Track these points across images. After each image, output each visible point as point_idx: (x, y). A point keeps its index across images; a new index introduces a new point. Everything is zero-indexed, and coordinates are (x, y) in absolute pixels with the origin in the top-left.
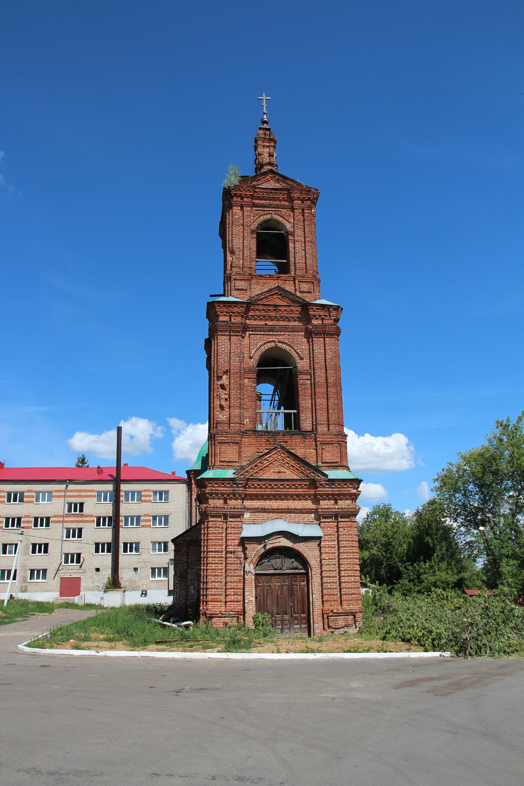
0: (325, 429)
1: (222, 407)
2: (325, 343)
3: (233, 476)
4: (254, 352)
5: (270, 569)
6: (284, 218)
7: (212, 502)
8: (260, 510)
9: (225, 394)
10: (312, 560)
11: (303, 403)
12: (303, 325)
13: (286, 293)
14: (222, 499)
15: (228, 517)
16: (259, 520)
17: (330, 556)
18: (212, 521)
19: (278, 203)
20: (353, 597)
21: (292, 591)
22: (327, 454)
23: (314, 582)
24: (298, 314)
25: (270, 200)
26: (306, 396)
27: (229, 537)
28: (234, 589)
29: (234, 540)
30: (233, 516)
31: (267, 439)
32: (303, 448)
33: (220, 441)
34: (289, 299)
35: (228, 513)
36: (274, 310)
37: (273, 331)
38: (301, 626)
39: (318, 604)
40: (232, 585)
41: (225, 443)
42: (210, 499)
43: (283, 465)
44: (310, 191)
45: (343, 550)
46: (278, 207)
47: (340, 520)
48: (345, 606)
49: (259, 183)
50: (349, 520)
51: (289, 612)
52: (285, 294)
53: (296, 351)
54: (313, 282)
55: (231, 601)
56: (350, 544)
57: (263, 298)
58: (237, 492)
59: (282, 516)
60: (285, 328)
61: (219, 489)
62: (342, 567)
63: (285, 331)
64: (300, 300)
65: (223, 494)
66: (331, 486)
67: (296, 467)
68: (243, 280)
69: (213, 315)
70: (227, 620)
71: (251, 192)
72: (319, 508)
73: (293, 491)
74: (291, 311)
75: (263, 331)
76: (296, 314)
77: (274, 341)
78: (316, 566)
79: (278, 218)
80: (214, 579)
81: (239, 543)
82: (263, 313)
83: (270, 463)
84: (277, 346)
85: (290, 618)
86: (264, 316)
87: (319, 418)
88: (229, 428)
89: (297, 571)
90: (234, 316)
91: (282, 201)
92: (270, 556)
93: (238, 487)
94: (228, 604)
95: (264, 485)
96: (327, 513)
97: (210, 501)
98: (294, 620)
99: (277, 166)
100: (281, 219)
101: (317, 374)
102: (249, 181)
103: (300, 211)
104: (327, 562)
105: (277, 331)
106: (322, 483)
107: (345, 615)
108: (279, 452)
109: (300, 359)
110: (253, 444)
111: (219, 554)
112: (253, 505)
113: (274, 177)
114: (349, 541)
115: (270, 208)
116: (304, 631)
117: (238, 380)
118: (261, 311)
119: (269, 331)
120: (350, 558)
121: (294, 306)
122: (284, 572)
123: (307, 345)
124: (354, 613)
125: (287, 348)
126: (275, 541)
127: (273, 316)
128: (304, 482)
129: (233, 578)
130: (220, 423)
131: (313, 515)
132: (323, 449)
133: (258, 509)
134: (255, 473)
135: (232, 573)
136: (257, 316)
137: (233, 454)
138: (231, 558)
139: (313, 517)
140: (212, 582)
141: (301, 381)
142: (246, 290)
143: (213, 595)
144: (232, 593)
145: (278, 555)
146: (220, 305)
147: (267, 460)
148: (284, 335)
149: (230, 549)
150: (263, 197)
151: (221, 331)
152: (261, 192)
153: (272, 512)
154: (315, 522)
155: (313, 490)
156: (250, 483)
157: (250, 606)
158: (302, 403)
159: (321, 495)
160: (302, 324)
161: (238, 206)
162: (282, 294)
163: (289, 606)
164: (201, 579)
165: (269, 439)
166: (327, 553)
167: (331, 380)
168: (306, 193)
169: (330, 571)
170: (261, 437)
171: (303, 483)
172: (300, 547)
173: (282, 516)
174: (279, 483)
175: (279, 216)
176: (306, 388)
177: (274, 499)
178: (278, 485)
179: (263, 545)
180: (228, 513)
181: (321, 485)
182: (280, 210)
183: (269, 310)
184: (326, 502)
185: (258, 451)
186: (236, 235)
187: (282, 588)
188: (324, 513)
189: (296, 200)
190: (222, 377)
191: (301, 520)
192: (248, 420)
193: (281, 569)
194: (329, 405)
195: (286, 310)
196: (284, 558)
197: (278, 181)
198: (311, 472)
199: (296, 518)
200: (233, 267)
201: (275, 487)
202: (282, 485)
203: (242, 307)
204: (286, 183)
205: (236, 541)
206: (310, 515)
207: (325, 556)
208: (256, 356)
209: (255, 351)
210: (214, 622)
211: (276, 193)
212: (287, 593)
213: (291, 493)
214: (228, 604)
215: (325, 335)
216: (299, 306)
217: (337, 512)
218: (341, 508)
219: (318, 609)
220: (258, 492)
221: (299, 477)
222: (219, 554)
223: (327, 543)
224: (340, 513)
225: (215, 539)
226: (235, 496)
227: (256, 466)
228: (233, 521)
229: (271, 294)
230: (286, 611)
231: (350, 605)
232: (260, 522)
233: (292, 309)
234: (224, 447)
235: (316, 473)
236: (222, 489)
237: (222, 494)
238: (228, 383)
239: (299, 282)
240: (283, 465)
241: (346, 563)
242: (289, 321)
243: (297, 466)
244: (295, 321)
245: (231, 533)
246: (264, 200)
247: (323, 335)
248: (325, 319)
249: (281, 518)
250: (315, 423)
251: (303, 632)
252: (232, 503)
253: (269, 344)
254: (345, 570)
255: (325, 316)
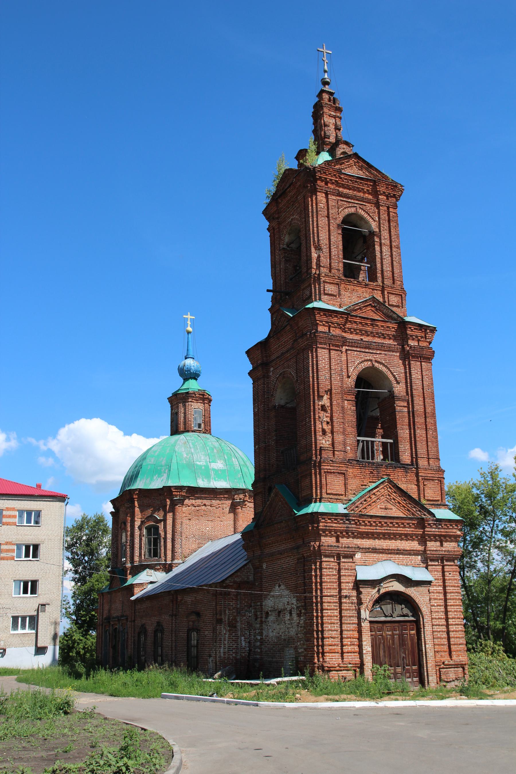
0: (426, 463)
1: (324, 432)
2: (422, 368)
3: (346, 511)
4: (352, 370)
5: (381, 615)
6: (369, 214)
7: (324, 539)
8: (370, 550)
9: (327, 417)
10: (423, 607)
11: (401, 433)
12: (397, 345)
13: (380, 306)
14: (334, 536)
15: (341, 557)
16: (370, 561)
17: (438, 602)
18: (326, 561)
19: (361, 194)
20: (461, 648)
21: (403, 640)
22: (429, 491)
23: (426, 631)
24: (394, 331)
25: (354, 190)
26: (403, 425)
27: (343, 579)
28: (350, 638)
29: (348, 583)
30: (345, 557)
31: (371, 470)
32: (405, 482)
33: (326, 470)
34: (383, 313)
35: (342, 552)
36: (372, 325)
37: (369, 348)
38: (412, 680)
39: (431, 655)
40: (348, 634)
41: (331, 473)
42: (323, 536)
43: (389, 501)
44: (396, 186)
45: (450, 596)
46: (362, 200)
47: (445, 563)
48: (454, 657)
49: (343, 166)
50: (453, 563)
51: (401, 664)
52: (379, 307)
53: (392, 373)
54: (401, 295)
55: (348, 652)
56: (456, 589)
57: (358, 309)
58: (351, 529)
59: (391, 557)
60: (382, 346)
61: (332, 525)
62: (450, 615)
63: (381, 350)
64: (395, 316)
65: (336, 531)
66: (437, 526)
67: (402, 503)
68: (332, 283)
69: (309, 323)
70: (345, 673)
71: (336, 178)
72: (428, 550)
73: (401, 530)
74: (388, 327)
75: (360, 347)
76: (392, 331)
77: (371, 360)
78: (428, 613)
79: (363, 213)
80: (331, 627)
81: (353, 586)
82: (360, 327)
83: (377, 498)
84: (373, 365)
85: (402, 670)
86: (361, 330)
87: (419, 451)
88: (334, 456)
89: (407, 619)
90: (333, 327)
91: (366, 193)
92: (381, 602)
93: (350, 524)
94: (346, 656)
95: (374, 522)
96: (435, 556)
97: (322, 538)
98: (406, 673)
99: (353, 146)
100: (366, 216)
101: (415, 402)
102: (333, 163)
103: (386, 208)
104: (436, 609)
105: (373, 349)
106: (430, 522)
107: (454, 668)
108: (386, 486)
109: (397, 383)
110: (358, 475)
111: (334, 599)
112: (363, 544)
113: (358, 162)
114: (454, 586)
115: (354, 199)
116: (416, 685)
117: (340, 401)
118: (358, 324)
119: (365, 348)
120: (457, 605)
121: (391, 322)
122: (394, 619)
123: (402, 368)
124: (462, 665)
125: (384, 369)
126: (387, 585)
127: (369, 331)
128: (412, 520)
129: (348, 626)
130: (325, 450)
131: (420, 557)
132: (424, 485)
133: (369, 549)
134: (364, 509)
135: (347, 620)
136: (354, 329)
137: (340, 486)
138: (346, 603)
139: (420, 559)
140: (329, 630)
141: (399, 408)
142: (336, 296)
143: (330, 645)
144: (349, 643)
145: (388, 601)
146: (320, 313)
147: (375, 495)
148: (380, 354)
149: (345, 593)
150: (347, 185)
151: (321, 343)
152: (346, 179)
153: (382, 553)
154: (422, 565)
155: (421, 530)
156: (361, 519)
157: (368, 657)
158: (400, 433)
159: (429, 536)
160: (396, 344)
161: (322, 192)
162: (376, 306)
163: (400, 657)
164: (314, 627)
165: (372, 471)
166: (435, 599)
167: (429, 410)
168: (392, 189)
169: (439, 618)
170: (365, 468)
171: (411, 522)
172: (412, 592)
173: (391, 557)
174: (383, 521)
175: (364, 211)
176: (403, 417)
177: (383, 539)
178: (394, 523)
179: (377, 589)
180: (342, 552)
181: (429, 524)
182: (364, 204)
183: (366, 324)
184: (432, 543)
185: (362, 483)
186: (322, 228)
187: (394, 637)
188: (432, 556)
189: (381, 194)
190: (322, 397)
191: (409, 562)
192: (349, 448)
193: (392, 616)
194: (428, 437)
195: (382, 326)
196: (395, 604)
197: (361, 168)
198: (418, 510)
199: (404, 560)
200: (321, 266)
201: (384, 525)
202: (391, 523)
203: (342, 317)
204: (370, 172)
205: (350, 585)
206: (417, 557)
207: (434, 602)
208: (354, 375)
209: (353, 370)
210: (332, 676)
211: (361, 183)
212: (398, 642)
213: (400, 532)
214: (346, 656)
215: (422, 359)
216: (396, 323)
217: (444, 554)
218: (448, 551)
219: (431, 661)
220: (369, 530)
221: (405, 514)
222: (334, 599)
223: (435, 588)
224: (446, 556)
225: (330, 582)
226: (348, 534)
227: (365, 501)
228: (347, 562)
229: (366, 304)
230: (398, 663)
231: (459, 656)
232: (370, 563)
233: (389, 325)
234: (330, 478)
235: (423, 511)
236: (334, 525)
237: (336, 531)
238: (329, 404)
239: (388, 293)
240: (389, 501)
241: (453, 610)
242: (385, 338)
243: (403, 503)
244: (390, 339)
245: (345, 576)
246: (348, 189)
247: (419, 358)
248: (420, 341)
249: (390, 560)
250: (414, 456)
251: (415, 687)
252: (344, 541)
253: (366, 363)
254: (453, 618)
255: (422, 337)
